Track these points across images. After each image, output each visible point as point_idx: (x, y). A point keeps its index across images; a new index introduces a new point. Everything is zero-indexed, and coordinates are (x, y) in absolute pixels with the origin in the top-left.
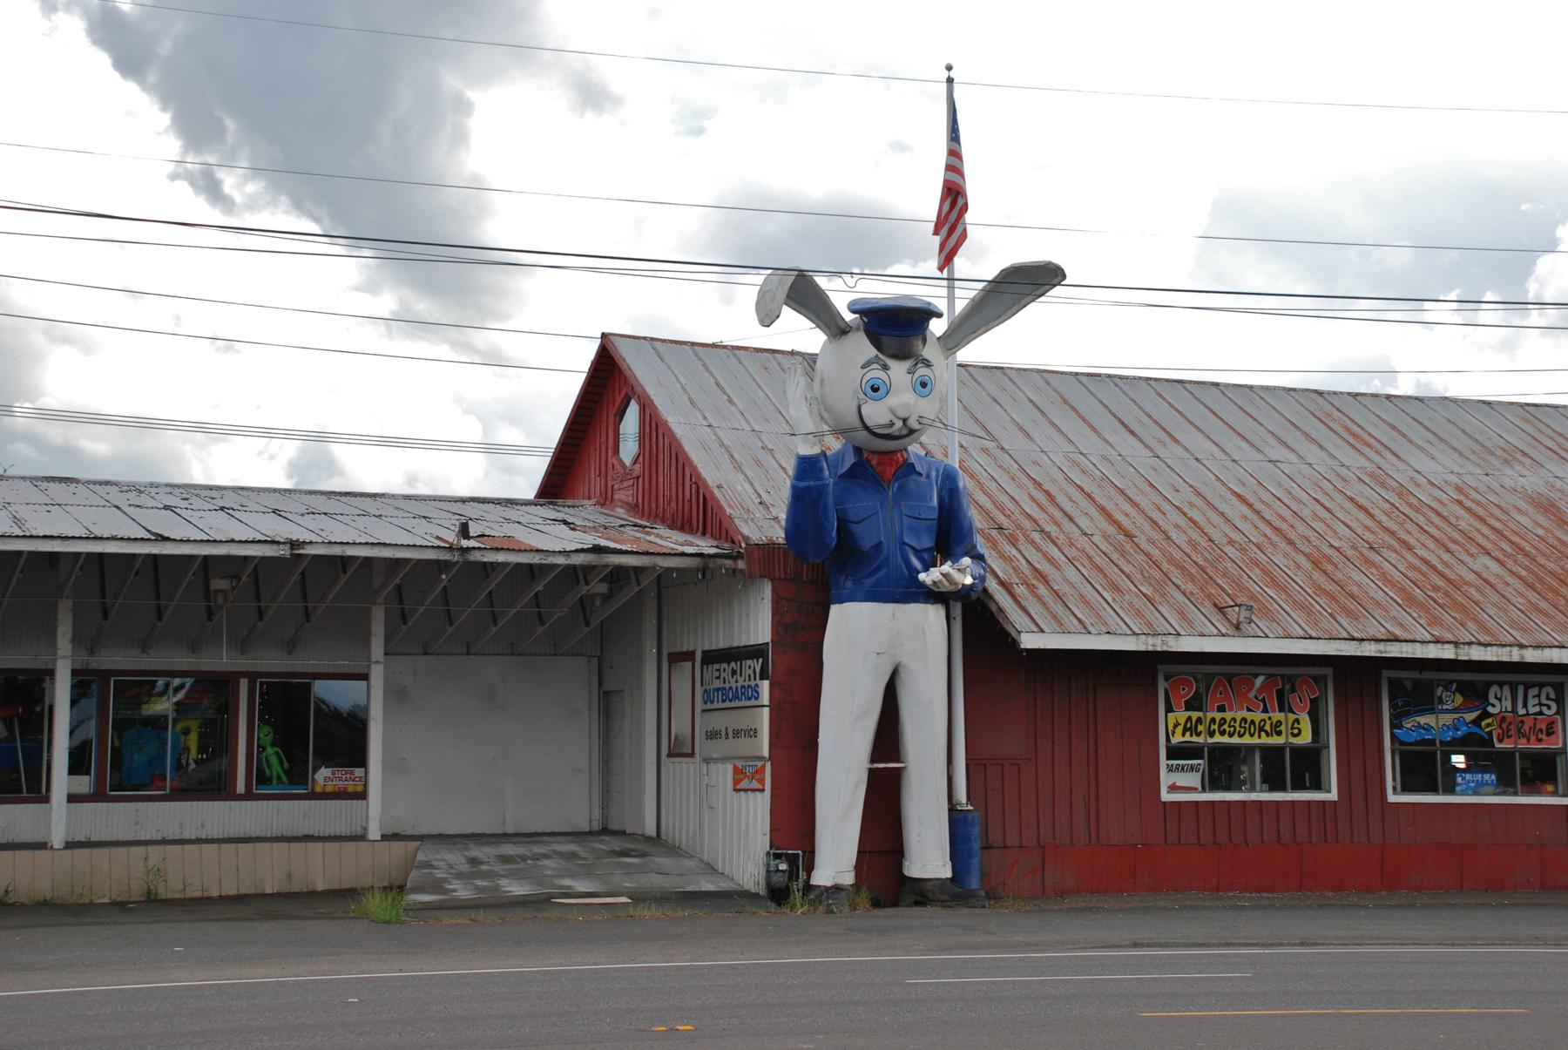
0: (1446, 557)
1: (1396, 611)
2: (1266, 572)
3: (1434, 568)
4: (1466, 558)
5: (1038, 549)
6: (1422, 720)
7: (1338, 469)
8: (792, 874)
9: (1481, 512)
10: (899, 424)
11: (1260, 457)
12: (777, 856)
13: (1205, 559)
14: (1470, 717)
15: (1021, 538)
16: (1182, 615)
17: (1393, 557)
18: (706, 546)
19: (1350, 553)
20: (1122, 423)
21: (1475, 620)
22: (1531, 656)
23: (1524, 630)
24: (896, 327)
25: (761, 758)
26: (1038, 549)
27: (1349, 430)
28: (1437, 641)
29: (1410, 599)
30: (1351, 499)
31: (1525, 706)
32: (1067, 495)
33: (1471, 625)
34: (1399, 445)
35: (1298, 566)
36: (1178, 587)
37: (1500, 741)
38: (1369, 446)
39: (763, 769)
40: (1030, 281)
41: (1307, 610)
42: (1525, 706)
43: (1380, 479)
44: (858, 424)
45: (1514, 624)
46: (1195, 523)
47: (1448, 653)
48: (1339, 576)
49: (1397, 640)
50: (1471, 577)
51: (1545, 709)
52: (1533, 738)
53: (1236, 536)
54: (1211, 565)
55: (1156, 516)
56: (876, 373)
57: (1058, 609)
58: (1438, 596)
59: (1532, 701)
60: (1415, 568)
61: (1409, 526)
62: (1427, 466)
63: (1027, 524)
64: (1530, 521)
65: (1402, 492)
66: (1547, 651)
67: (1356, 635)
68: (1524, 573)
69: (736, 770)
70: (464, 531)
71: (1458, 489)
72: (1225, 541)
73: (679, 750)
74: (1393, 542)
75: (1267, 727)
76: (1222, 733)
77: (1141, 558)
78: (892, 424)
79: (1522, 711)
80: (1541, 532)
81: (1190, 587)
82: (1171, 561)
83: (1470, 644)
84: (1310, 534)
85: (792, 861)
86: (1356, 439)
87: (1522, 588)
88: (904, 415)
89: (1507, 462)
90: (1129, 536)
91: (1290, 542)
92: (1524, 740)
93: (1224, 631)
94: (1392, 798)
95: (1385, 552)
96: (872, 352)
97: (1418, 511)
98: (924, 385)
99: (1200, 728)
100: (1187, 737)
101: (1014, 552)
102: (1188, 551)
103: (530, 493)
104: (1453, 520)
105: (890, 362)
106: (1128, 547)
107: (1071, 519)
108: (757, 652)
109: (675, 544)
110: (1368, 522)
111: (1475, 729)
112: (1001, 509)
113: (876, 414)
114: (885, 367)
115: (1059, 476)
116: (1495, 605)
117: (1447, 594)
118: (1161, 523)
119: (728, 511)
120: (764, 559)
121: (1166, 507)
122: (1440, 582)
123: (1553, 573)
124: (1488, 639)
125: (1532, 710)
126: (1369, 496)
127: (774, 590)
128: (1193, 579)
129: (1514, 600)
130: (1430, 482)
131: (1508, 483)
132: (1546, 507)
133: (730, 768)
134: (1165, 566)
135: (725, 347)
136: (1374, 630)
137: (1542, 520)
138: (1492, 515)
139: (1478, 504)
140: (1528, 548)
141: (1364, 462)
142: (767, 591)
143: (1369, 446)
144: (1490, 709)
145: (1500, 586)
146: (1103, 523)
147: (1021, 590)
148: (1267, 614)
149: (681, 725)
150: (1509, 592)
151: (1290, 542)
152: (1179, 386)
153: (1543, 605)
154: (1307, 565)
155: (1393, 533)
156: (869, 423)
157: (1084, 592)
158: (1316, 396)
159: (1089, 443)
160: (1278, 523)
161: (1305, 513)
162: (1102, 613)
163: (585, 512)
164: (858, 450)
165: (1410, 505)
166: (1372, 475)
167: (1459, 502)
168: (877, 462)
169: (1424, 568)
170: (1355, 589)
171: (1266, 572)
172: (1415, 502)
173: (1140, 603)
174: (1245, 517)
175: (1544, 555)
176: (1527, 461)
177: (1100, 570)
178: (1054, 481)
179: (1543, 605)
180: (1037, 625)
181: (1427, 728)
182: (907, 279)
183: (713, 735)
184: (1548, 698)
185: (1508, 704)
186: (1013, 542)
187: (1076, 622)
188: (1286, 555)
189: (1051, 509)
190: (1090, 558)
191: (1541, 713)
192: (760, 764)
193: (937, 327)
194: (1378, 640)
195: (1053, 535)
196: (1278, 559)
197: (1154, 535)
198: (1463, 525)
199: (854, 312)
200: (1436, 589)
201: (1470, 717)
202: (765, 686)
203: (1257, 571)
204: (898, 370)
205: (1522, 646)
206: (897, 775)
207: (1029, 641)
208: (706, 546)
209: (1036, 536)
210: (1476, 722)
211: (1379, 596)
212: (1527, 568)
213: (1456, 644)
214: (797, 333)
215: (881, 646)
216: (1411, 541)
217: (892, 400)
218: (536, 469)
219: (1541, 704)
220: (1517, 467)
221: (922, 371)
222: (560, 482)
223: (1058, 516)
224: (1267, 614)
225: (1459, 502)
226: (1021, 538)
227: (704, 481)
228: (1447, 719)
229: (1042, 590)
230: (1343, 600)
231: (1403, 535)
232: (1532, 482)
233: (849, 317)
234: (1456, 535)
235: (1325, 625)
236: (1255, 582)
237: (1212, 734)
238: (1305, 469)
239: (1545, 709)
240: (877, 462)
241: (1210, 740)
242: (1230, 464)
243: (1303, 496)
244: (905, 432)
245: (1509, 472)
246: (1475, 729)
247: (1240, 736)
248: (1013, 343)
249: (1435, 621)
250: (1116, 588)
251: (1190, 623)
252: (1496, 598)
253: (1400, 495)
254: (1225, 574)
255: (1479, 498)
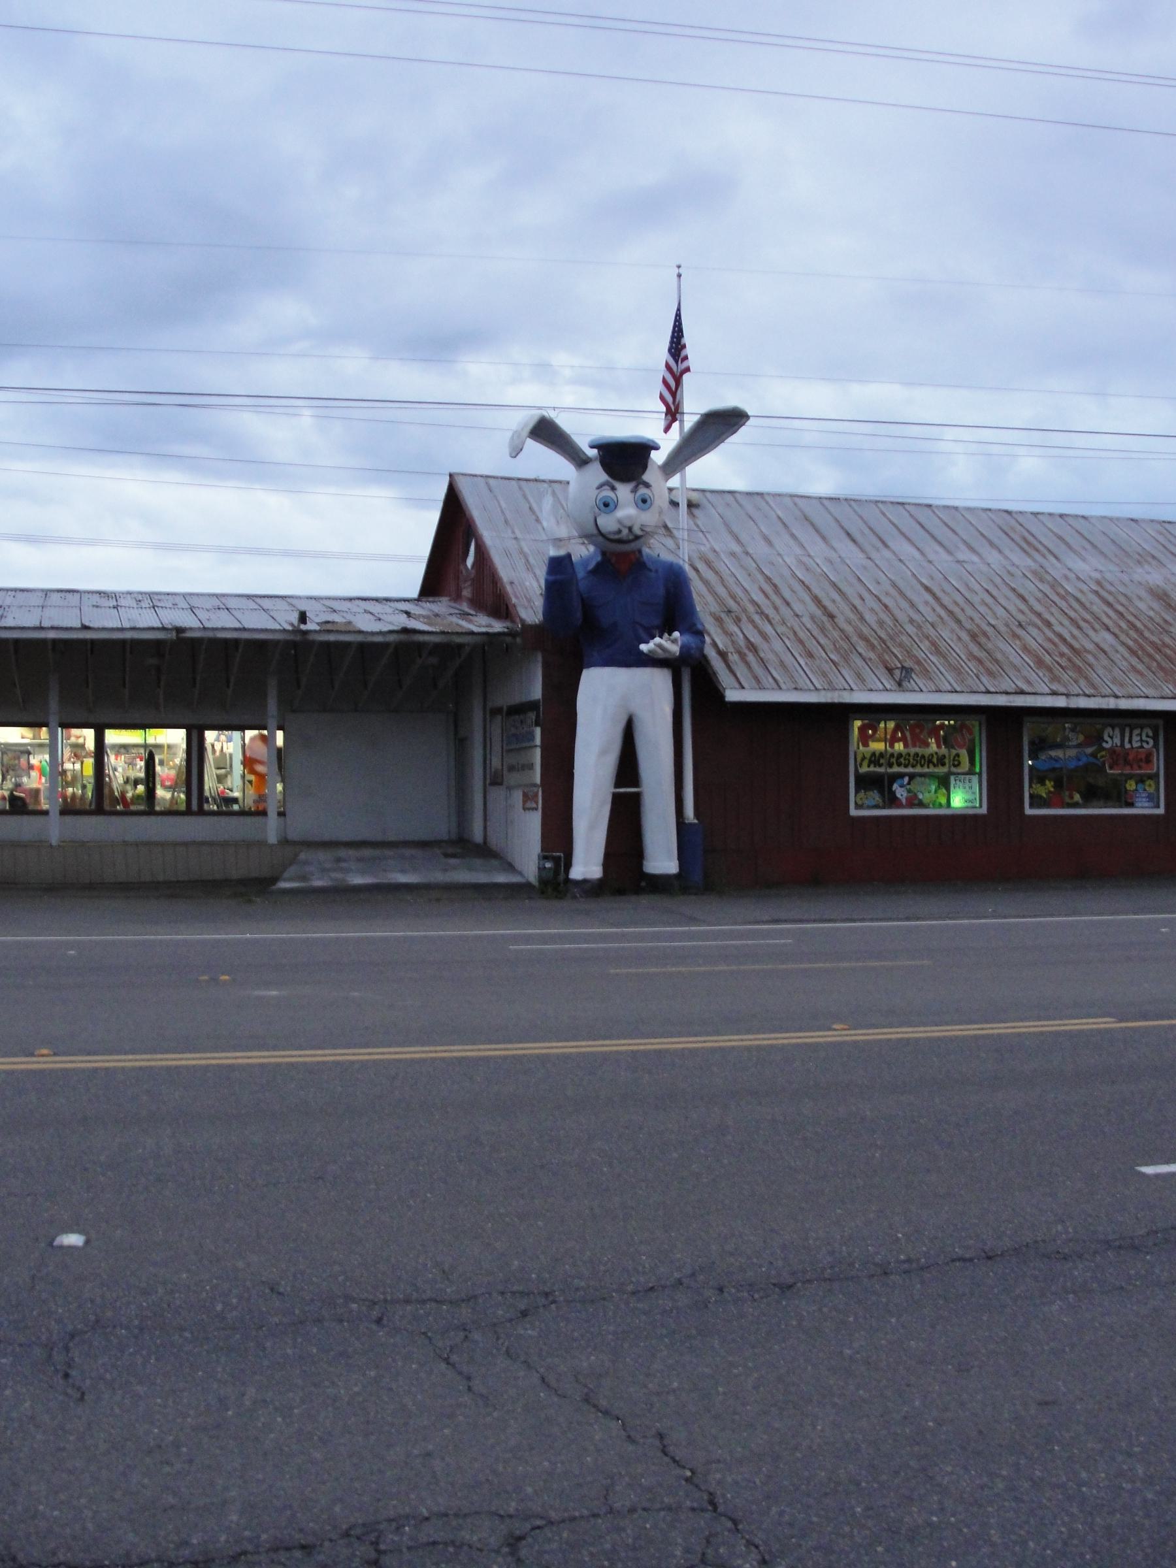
0: (1076, 632)
1: (1027, 672)
2: (933, 644)
3: (1064, 640)
4: (1091, 633)
5: (756, 627)
6: (1053, 753)
7: (1010, 568)
8: (556, 871)
9: (1111, 599)
10: (625, 532)
11: (949, 558)
12: (545, 858)
13: (889, 635)
14: (1089, 750)
15: (744, 619)
16: (859, 676)
17: (1034, 632)
18: (498, 626)
19: (1003, 629)
20: (848, 534)
21: (1086, 678)
22: (1124, 704)
23: (1122, 685)
24: (624, 460)
25: (535, 785)
26: (756, 627)
27: (1025, 539)
28: (1054, 693)
29: (1040, 662)
30: (1014, 590)
31: (1130, 742)
32: (790, 587)
33: (1082, 683)
34: (1060, 549)
35: (959, 638)
36: (860, 654)
37: (1111, 768)
38: (1037, 550)
39: (536, 795)
40: (722, 423)
41: (957, 671)
42: (1130, 742)
43: (1040, 575)
44: (595, 532)
45: (1114, 680)
46: (886, 607)
47: (1061, 702)
48: (990, 646)
49: (1022, 692)
50: (1090, 646)
51: (1145, 745)
52: (1135, 766)
53: (916, 617)
54: (892, 639)
55: (857, 602)
56: (607, 493)
57: (759, 671)
58: (1063, 662)
59: (1135, 738)
60: (1050, 640)
61: (1054, 610)
62: (1079, 566)
63: (751, 609)
64: (1146, 606)
65: (1055, 585)
66: (1039, 698)
67: (992, 690)
68: (1131, 643)
69: (525, 795)
70: (303, 618)
71: (1098, 583)
72: (907, 619)
73: (495, 780)
74: (1039, 623)
75: (935, 760)
76: (899, 765)
77: (836, 634)
78: (620, 531)
79: (1127, 746)
80: (1152, 614)
81: (872, 655)
82: (862, 637)
83: (1078, 695)
84: (976, 616)
85: (556, 861)
86: (1029, 544)
87: (1127, 655)
88: (629, 524)
89: (1139, 562)
90: (832, 617)
91: (958, 622)
92: (1128, 767)
93: (888, 687)
94: (1029, 811)
95: (1030, 629)
96: (604, 477)
97: (1063, 598)
98: (644, 501)
99: (882, 761)
100: (872, 769)
101: (736, 629)
102: (875, 627)
103: (414, 592)
104: (1088, 605)
105: (617, 485)
106: (828, 625)
107: (788, 604)
108: (533, 706)
109: (483, 624)
110: (1023, 607)
111: (1092, 760)
112: (734, 597)
113: (608, 523)
114: (613, 489)
115: (786, 573)
116: (1105, 668)
117: (1070, 660)
118: (859, 607)
119: (514, 600)
120: (535, 637)
121: (866, 595)
122: (1066, 650)
123: (1152, 643)
124: (1092, 691)
125: (1135, 745)
126: (1029, 588)
127: (543, 657)
128: (873, 647)
129: (1119, 664)
130: (1078, 578)
131: (1136, 577)
132: (1161, 596)
133: (521, 794)
134: (855, 639)
135: (544, 481)
136: (1007, 685)
137: (1155, 605)
138: (1118, 601)
139: (1110, 593)
140: (1139, 624)
141: (1029, 562)
142: (540, 658)
143: (1037, 550)
144: (1104, 745)
145: (1112, 654)
146: (813, 608)
147: (734, 658)
148: (926, 673)
149: (496, 762)
150: (1117, 657)
151: (958, 622)
152: (900, 507)
153: (1140, 667)
154: (965, 636)
155: (1039, 615)
156: (603, 530)
157: (783, 657)
158: (1005, 515)
159: (817, 549)
160: (951, 607)
161: (976, 600)
162: (795, 674)
163: (440, 605)
164: (604, 554)
165: (1058, 594)
166: (1035, 573)
167: (1096, 593)
168: (621, 559)
169: (1056, 640)
170: (999, 656)
171: (933, 644)
172: (1063, 592)
173: (827, 667)
174: (927, 603)
175: (1149, 629)
176: (1154, 563)
177: (801, 642)
178: (782, 576)
179: (1140, 667)
180: (740, 683)
181: (1056, 760)
182: (645, 423)
183: (512, 769)
184: (1148, 736)
185: (1117, 741)
186: (737, 621)
187: (771, 680)
188: (952, 631)
189: (774, 597)
190: (795, 633)
191: (1142, 747)
192: (535, 789)
193: (658, 457)
194: (1007, 693)
195: (771, 616)
196: (945, 634)
197: (852, 616)
198: (1095, 608)
199: (592, 447)
200: (1062, 655)
201: (1089, 750)
202: (538, 731)
203: (927, 643)
204: (624, 491)
205: (1117, 697)
206: (636, 799)
207: (733, 695)
208: (498, 626)
209: (756, 618)
210: (1094, 755)
211: (1017, 661)
212: (1135, 641)
213: (1067, 695)
214: (544, 461)
215: (619, 700)
216: (1053, 620)
217: (620, 513)
218: (418, 571)
219: (1141, 741)
220: (1146, 566)
221: (642, 491)
222: (432, 585)
223: (778, 602)
224: (926, 673)
225: (1096, 593)
226: (744, 619)
227: (500, 579)
228: (1072, 753)
229: (751, 657)
230: (989, 665)
231: (1047, 616)
232: (1155, 577)
233: (592, 453)
234: (1088, 617)
235: (970, 682)
236: (923, 650)
237: (891, 765)
238: (985, 568)
239: (1145, 745)
240: (621, 559)
241: (890, 770)
242: (925, 564)
243: (977, 587)
244: (631, 537)
245: (1140, 570)
246: (1092, 760)
247: (913, 766)
248: (712, 470)
249: (1055, 679)
250: (810, 655)
251: (863, 681)
252: (1105, 662)
253: (1052, 587)
254: (901, 645)
255: (1113, 589)
